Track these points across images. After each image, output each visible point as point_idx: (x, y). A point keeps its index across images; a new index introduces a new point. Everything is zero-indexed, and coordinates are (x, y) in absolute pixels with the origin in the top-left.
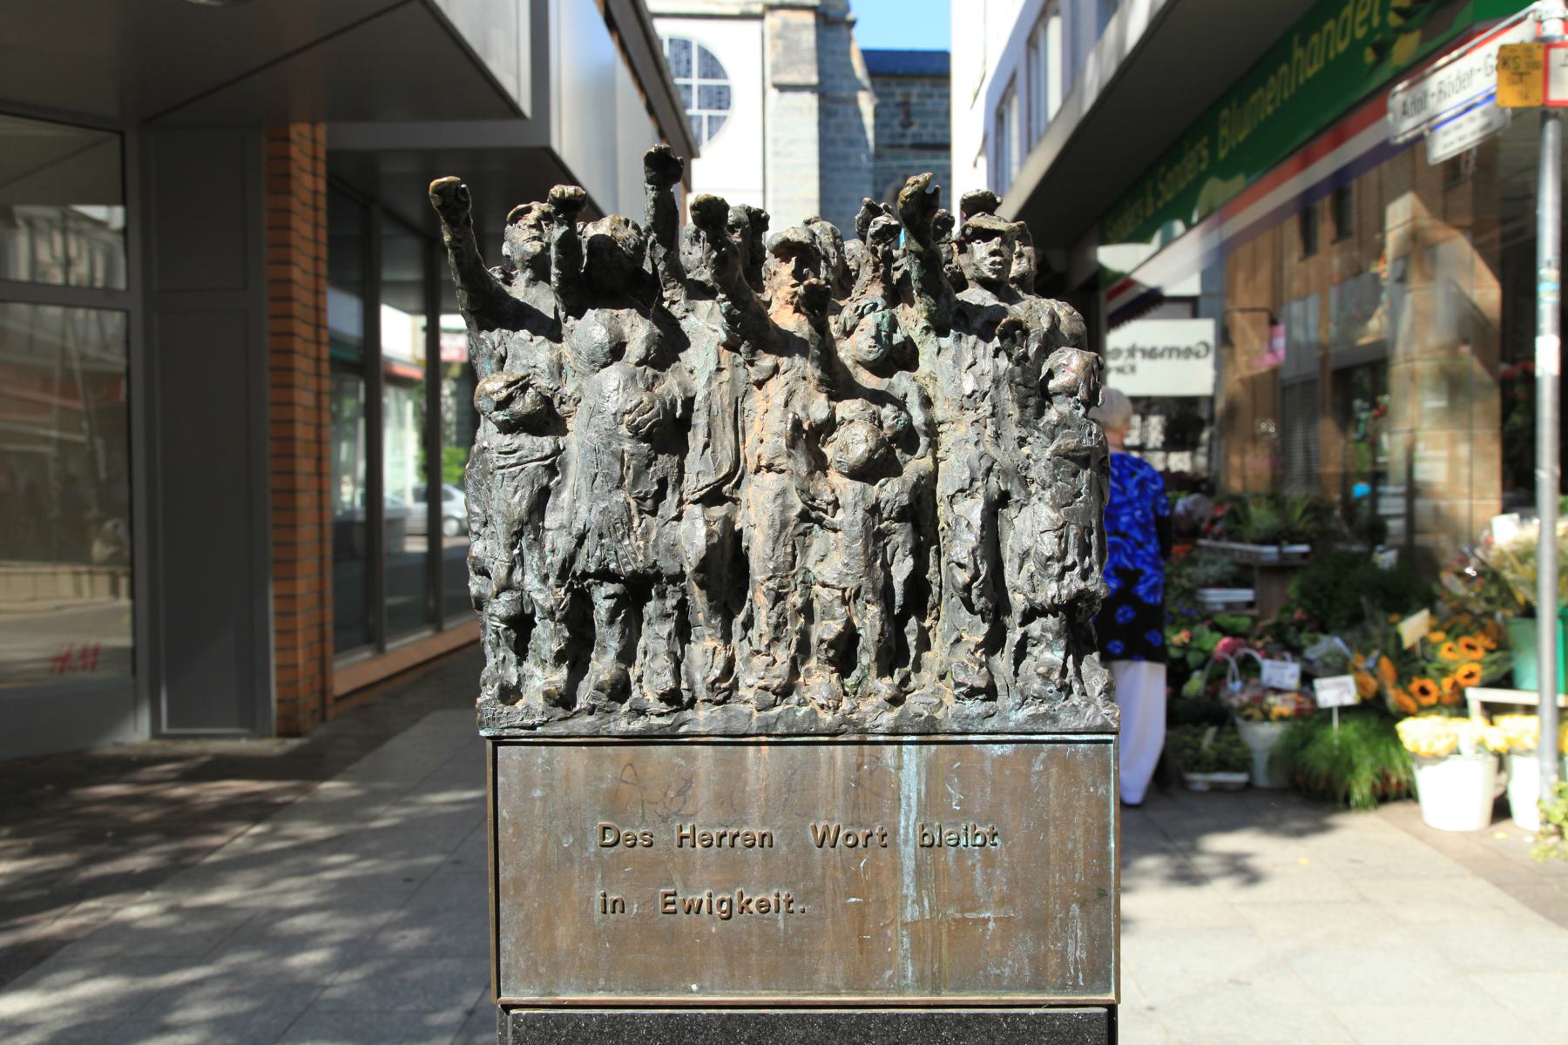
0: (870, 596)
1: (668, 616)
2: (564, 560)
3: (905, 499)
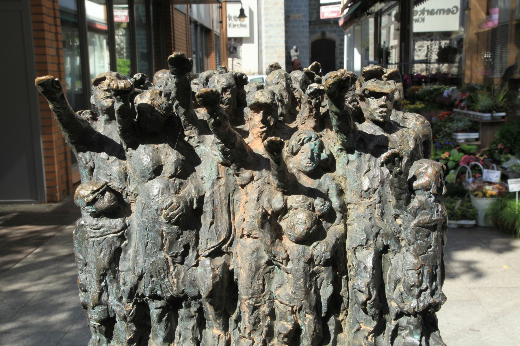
0: (308, 310)
1: (193, 317)
2: (131, 289)
3: (328, 255)
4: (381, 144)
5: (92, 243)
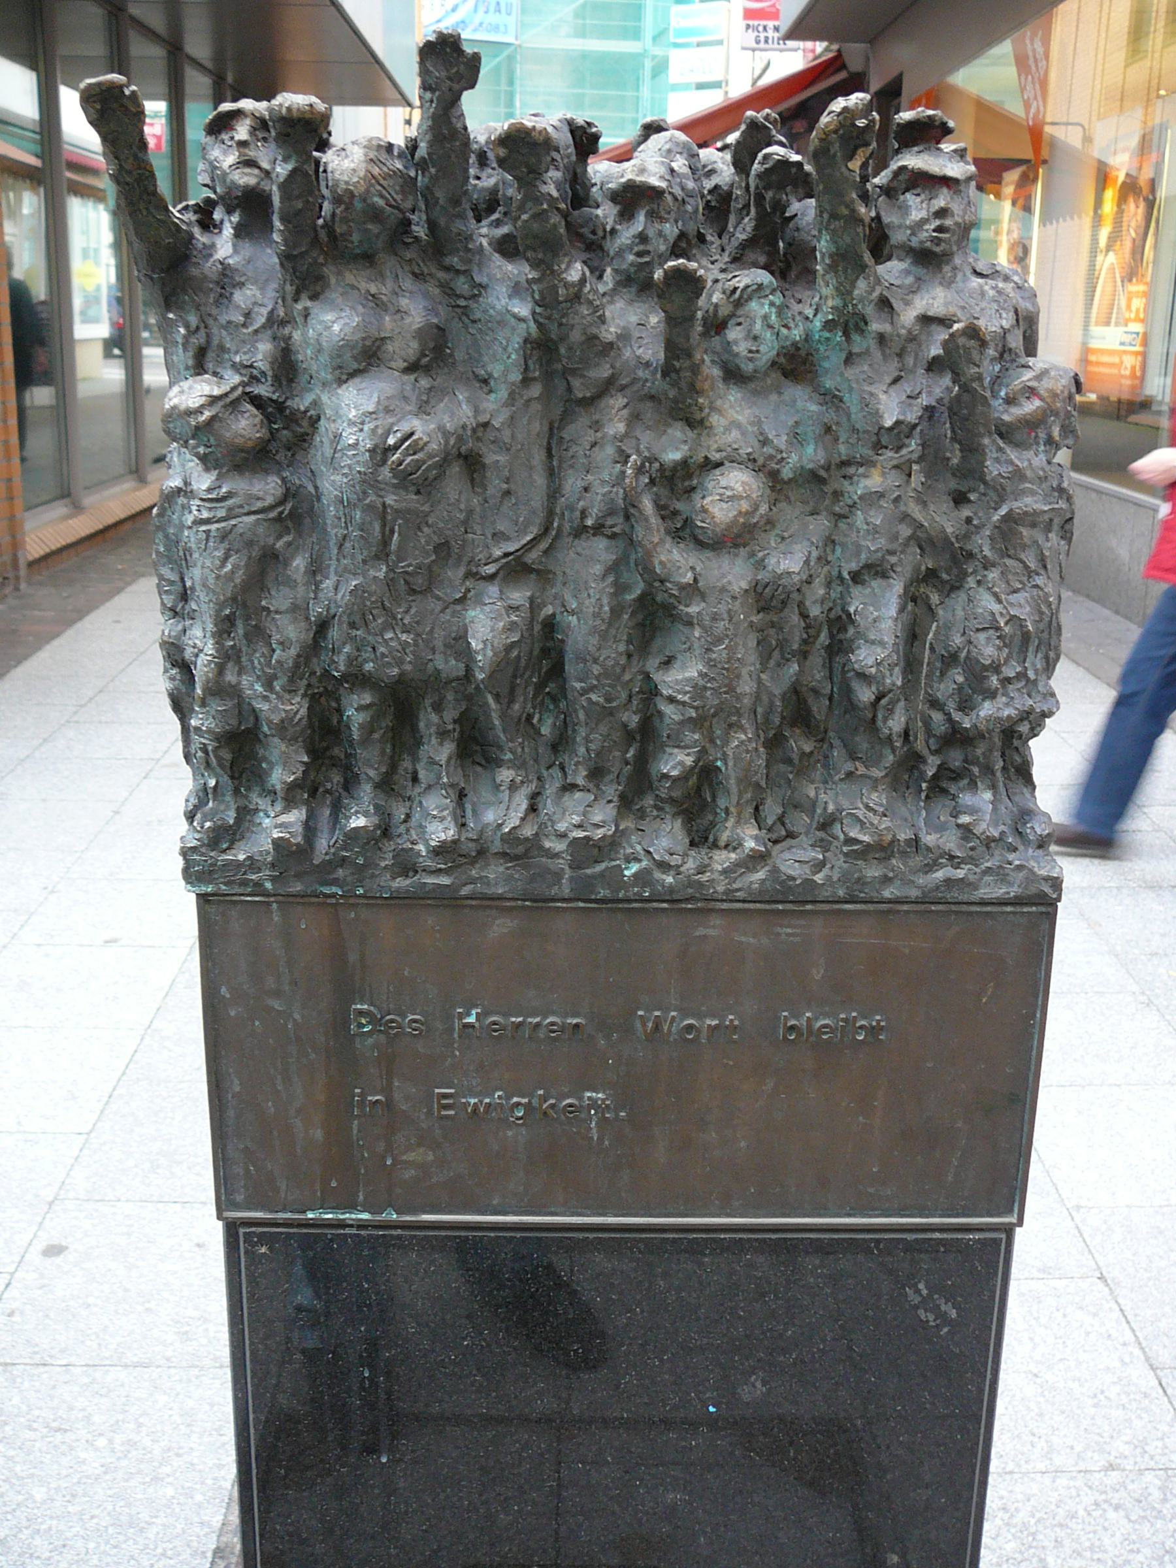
4: (930, 314)
5: (204, 535)
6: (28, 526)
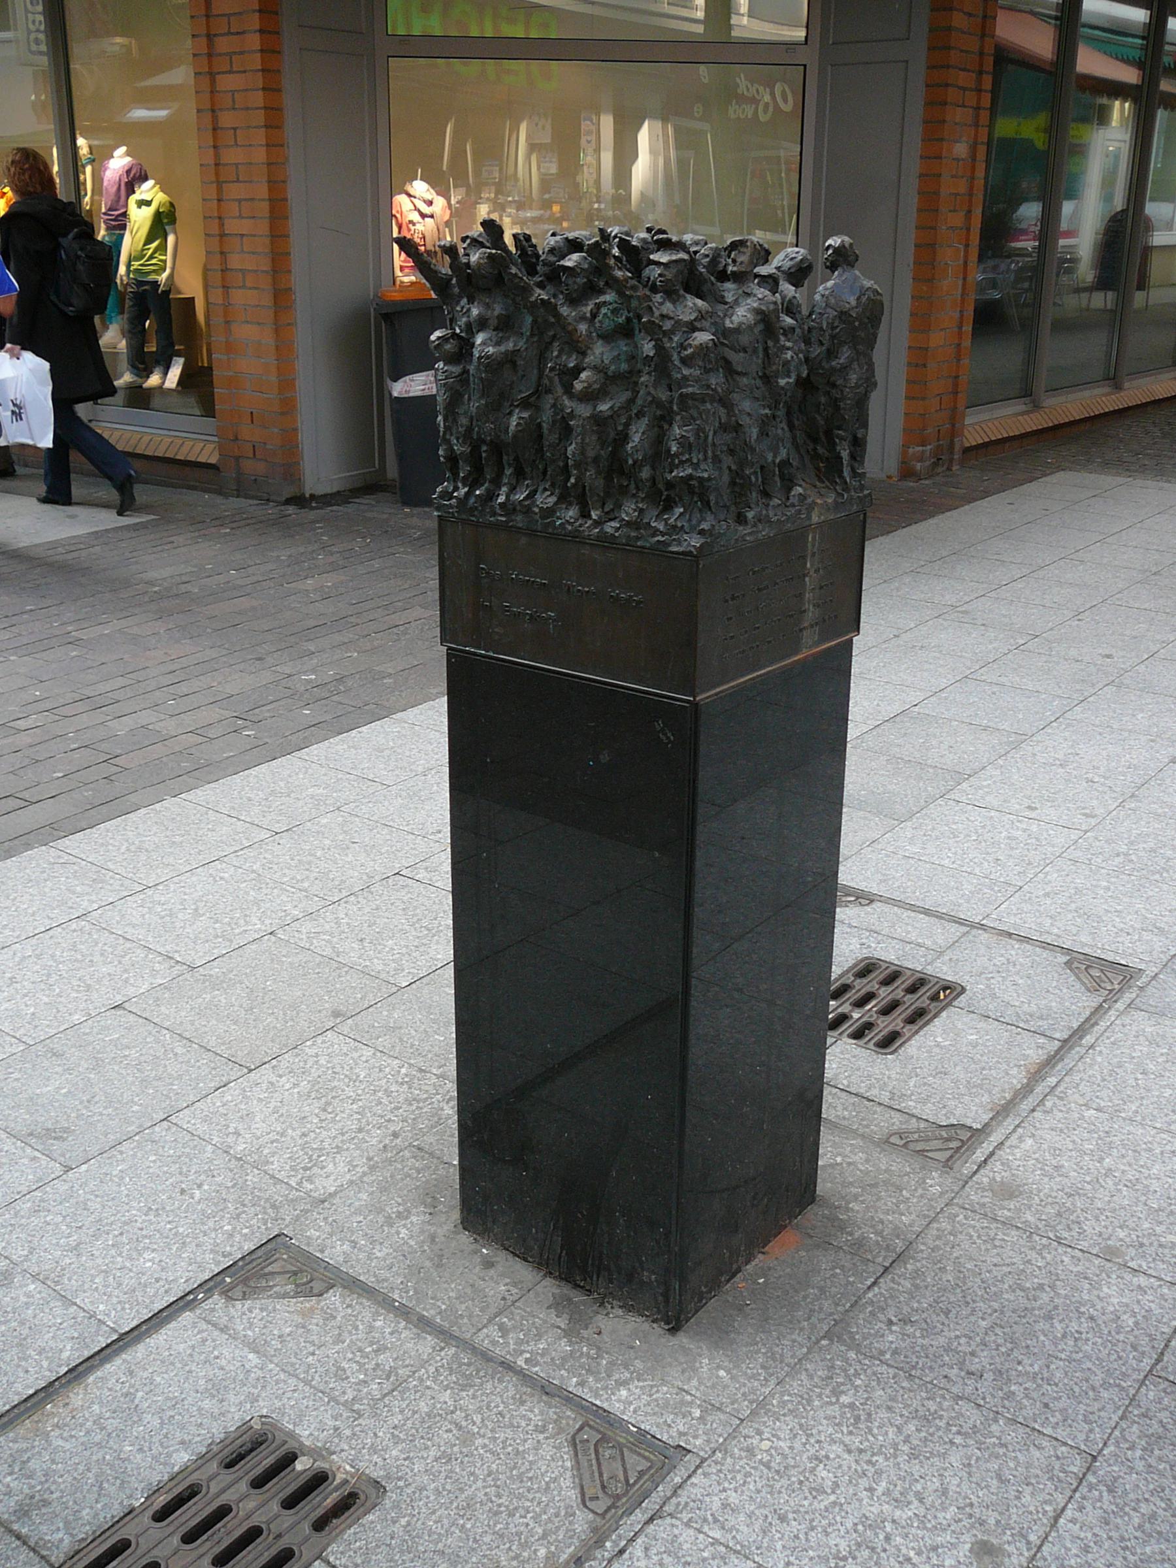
6: (968, 421)
